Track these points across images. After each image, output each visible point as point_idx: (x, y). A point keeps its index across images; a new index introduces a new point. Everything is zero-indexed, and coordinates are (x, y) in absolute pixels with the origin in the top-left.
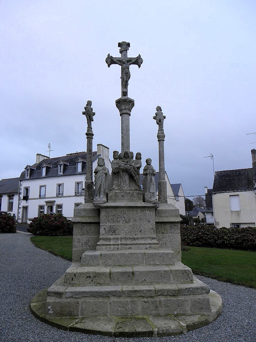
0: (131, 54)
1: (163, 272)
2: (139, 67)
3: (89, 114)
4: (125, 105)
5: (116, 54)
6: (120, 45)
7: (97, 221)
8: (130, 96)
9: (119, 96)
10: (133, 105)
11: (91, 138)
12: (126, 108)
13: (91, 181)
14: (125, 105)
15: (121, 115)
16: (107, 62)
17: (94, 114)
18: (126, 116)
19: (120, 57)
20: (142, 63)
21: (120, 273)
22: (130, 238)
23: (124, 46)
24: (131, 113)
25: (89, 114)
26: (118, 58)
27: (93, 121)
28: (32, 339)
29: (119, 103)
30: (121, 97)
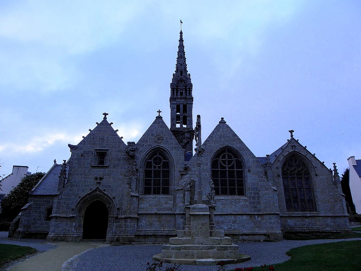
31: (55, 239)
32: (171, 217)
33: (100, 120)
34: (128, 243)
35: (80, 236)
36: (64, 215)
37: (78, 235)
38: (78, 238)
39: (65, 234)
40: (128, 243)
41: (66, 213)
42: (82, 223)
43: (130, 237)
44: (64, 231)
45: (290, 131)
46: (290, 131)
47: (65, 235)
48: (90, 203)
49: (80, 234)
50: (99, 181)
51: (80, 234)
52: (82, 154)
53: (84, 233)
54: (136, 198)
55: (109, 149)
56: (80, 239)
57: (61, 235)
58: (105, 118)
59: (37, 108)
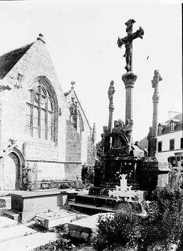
0: (135, 29)
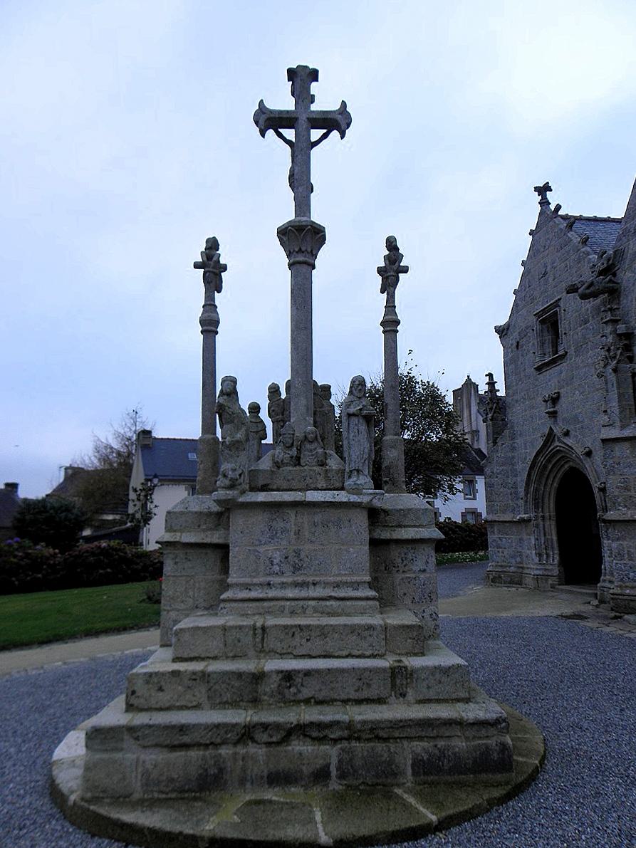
0: (324, 99)
1: (429, 810)
2: (342, 137)
3: (212, 268)
4: (302, 240)
5: (284, 101)
6: (292, 74)
7: (221, 541)
8: (317, 216)
9: (287, 214)
10: (322, 240)
11: (213, 331)
12: (303, 249)
13: (212, 436)
14: (302, 240)
15: (290, 266)
16: (257, 123)
17: (224, 268)
18: (304, 268)
19: (294, 109)
20: (348, 125)
21: (233, 673)
22: (557, 473)
23: (302, 78)
24: (317, 263)
25: (212, 268)
26: (288, 112)
27: (219, 293)
28: (10, 846)
29: (286, 234)
30: (292, 217)
31: (494, 577)
32: (23, 673)
33: (530, 216)
34: (613, 614)
35: (550, 574)
36: (508, 517)
37: (546, 573)
38: (547, 580)
39: (521, 565)
40: (613, 614)
41: (514, 510)
42: (555, 538)
43: (619, 591)
44: (518, 559)
45: (537, 189)
46: (537, 189)
47: (522, 568)
48: (559, 476)
49: (551, 567)
50: (552, 409)
51: (551, 567)
52: (518, 343)
53: (562, 563)
54: (627, 445)
55: (560, 299)
56: (550, 582)
57: (512, 569)
58: (544, 203)
59: (401, 317)
